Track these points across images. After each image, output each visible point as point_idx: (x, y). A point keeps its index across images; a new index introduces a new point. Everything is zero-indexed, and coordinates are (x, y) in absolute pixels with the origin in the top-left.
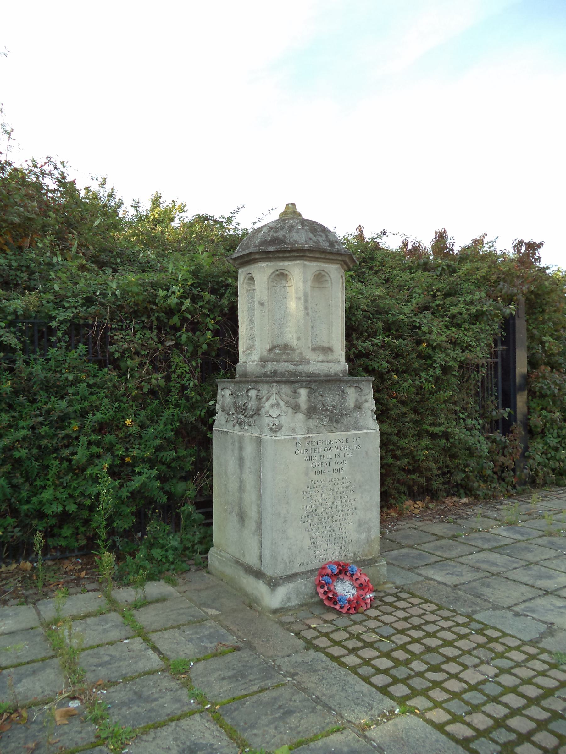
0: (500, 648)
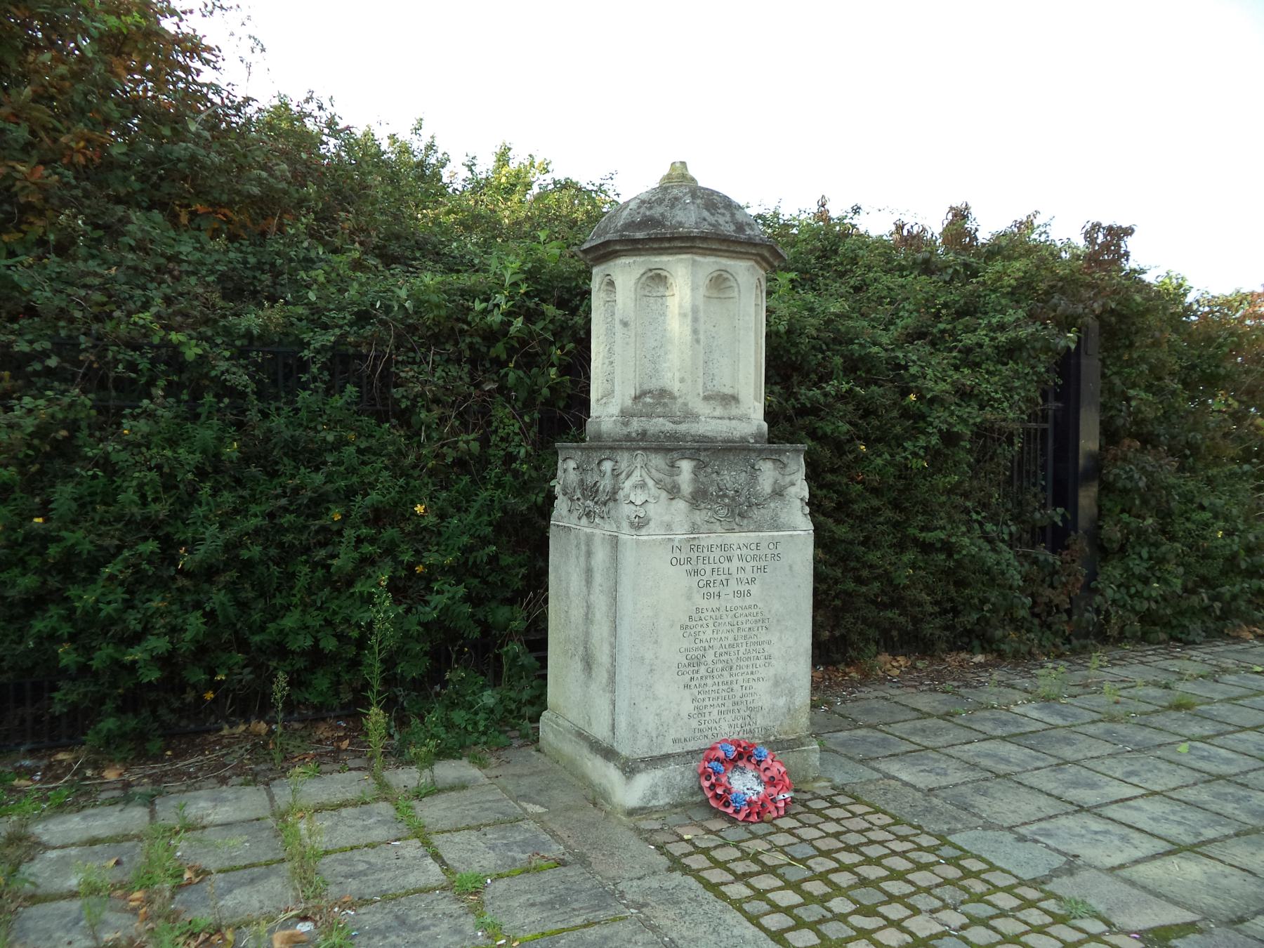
0: (978, 887)
